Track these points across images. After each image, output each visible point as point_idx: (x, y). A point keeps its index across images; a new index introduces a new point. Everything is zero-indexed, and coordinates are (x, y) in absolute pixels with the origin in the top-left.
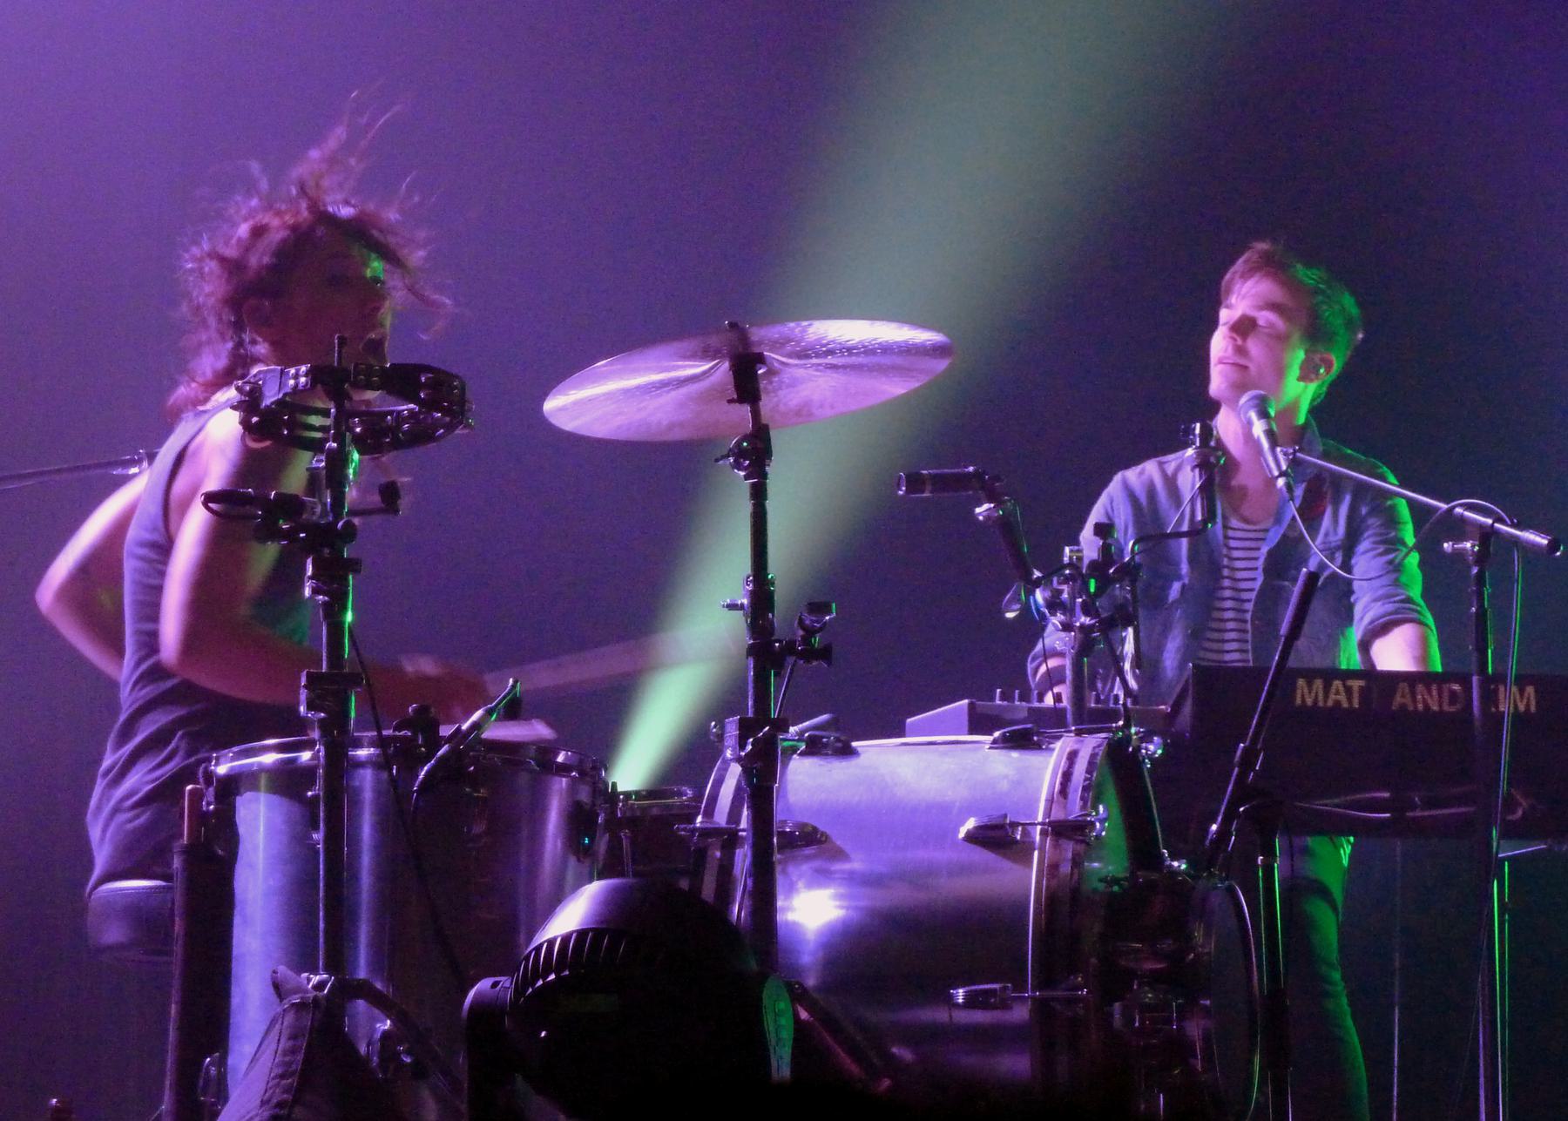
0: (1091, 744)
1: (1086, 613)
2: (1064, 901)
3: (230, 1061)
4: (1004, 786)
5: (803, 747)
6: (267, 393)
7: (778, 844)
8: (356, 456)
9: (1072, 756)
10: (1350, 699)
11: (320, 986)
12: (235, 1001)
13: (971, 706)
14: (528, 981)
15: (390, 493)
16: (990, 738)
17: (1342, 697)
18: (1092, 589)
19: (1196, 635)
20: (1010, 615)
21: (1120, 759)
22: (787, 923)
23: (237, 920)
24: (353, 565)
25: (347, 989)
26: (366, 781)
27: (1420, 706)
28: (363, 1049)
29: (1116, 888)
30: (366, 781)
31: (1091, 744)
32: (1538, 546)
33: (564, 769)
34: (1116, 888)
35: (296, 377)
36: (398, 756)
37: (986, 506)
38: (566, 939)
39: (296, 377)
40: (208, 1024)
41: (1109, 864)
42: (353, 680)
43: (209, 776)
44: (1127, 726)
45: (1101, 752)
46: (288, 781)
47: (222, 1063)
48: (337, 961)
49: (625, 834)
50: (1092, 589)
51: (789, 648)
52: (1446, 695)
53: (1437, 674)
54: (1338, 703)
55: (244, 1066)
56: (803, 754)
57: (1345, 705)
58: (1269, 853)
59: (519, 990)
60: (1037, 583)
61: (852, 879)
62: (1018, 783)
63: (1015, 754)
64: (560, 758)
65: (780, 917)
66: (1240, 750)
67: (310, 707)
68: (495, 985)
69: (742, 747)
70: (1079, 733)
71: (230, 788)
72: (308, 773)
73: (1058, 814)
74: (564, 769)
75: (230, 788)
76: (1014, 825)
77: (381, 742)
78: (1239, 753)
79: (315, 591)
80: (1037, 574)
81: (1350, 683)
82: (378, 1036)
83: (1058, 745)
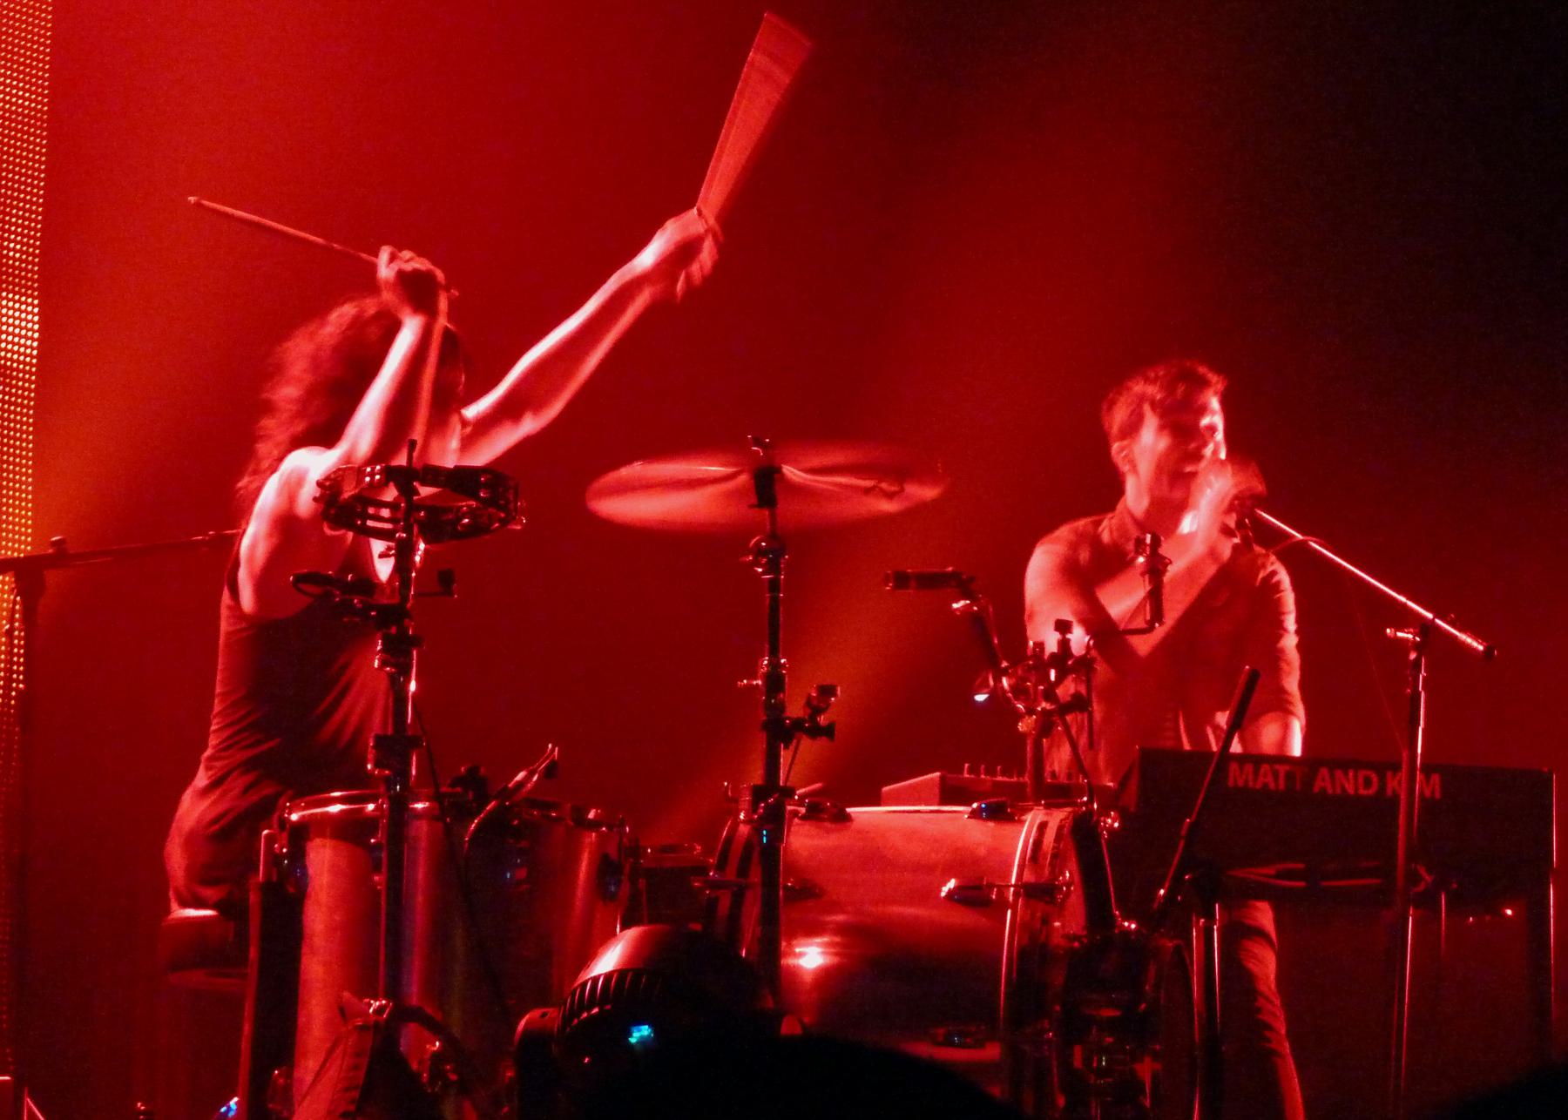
0: (1057, 818)
1: (1047, 700)
2: (1034, 952)
3: (296, 1075)
4: (982, 852)
5: (803, 810)
6: (346, 488)
7: (794, 902)
8: (422, 546)
9: (1043, 827)
10: (1276, 778)
11: (379, 1010)
12: (302, 1020)
13: (941, 777)
14: (574, 1012)
15: (446, 579)
16: (968, 809)
17: (1270, 779)
18: (1053, 678)
19: (1091, 719)
20: (980, 698)
21: (1082, 832)
22: (788, 966)
23: (305, 950)
24: (414, 642)
25: (402, 1013)
26: (422, 830)
27: (1339, 791)
28: (415, 1066)
29: (1076, 944)
30: (422, 830)
31: (1057, 818)
32: (1476, 650)
33: (594, 825)
34: (1076, 944)
35: (372, 475)
36: (451, 811)
37: (962, 603)
38: (608, 976)
39: (372, 475)
40: (278, 1042)
41: (1069, 924)
42: (413, 743)
43: (284, 823)
44: (1090, 802)
45: (1068, 824)
46: (349, 830)
47: (288, 1075)
48: (394, 991)
49: (642, 882)
50: (1053, 678)
51: (797, 724)
52: (1361, 781)
53: (1294, 758)
54: (1265, 784)
55: (309, 1078)
56: (804, 818)
57: (1272, 786)
58: (1210, 917)
59: (567, 1019)
60: (1004, 672)
61: (840, 930)
62: (993, 851)
63: (991, 824)
64: (591, 815)
65: (784, 962)
66: (1177, 826)
67: (376, 766)
68: (543, 1015)
69: (755, 812)
70: (1047, 807)
71: (300, 835)
72: (370, 824)
73: (1028, 876)
74: (594, 825)
75: (300, 835)
76: (991, 886)
77: (436, 798)
78: (1185, 827)
79: (383, 664)
80: (1004, 664)
81: (1277, 767)
82: (427, 1056)
83: (1029, 817)
